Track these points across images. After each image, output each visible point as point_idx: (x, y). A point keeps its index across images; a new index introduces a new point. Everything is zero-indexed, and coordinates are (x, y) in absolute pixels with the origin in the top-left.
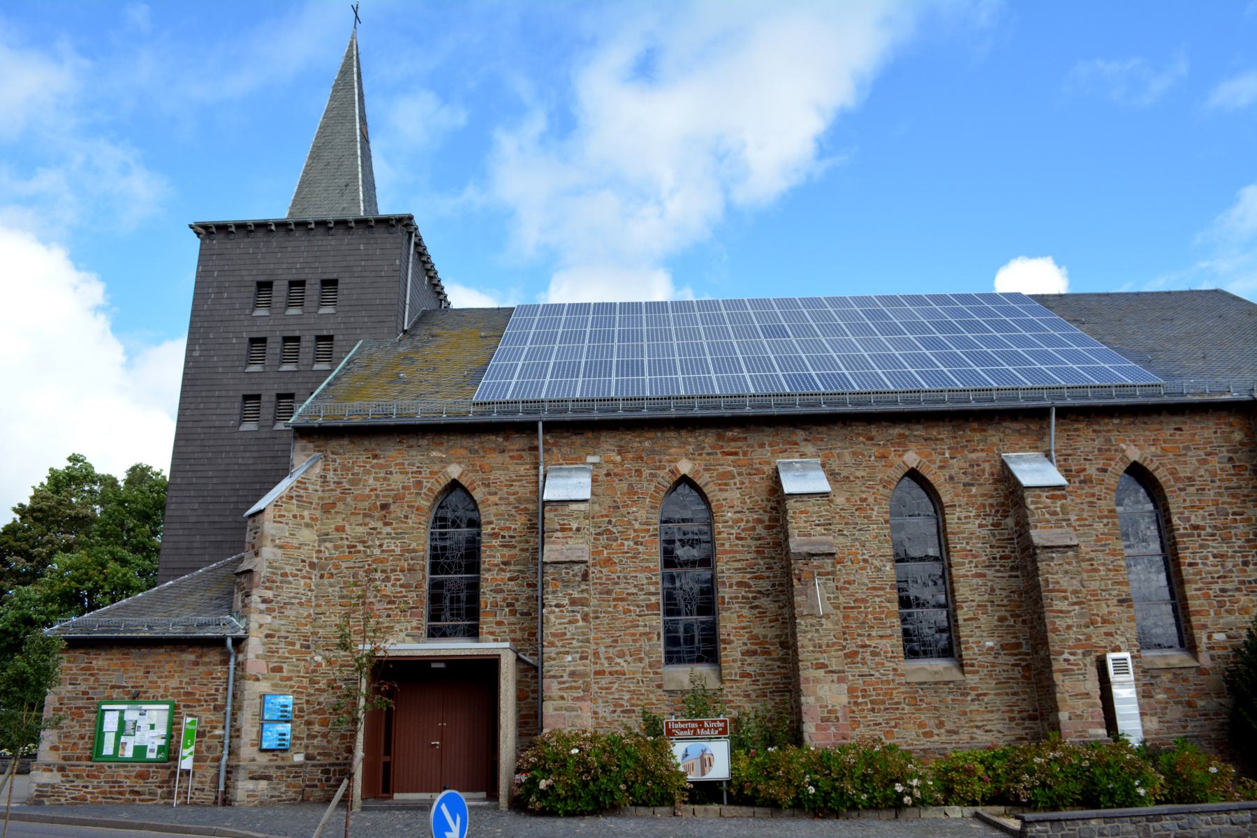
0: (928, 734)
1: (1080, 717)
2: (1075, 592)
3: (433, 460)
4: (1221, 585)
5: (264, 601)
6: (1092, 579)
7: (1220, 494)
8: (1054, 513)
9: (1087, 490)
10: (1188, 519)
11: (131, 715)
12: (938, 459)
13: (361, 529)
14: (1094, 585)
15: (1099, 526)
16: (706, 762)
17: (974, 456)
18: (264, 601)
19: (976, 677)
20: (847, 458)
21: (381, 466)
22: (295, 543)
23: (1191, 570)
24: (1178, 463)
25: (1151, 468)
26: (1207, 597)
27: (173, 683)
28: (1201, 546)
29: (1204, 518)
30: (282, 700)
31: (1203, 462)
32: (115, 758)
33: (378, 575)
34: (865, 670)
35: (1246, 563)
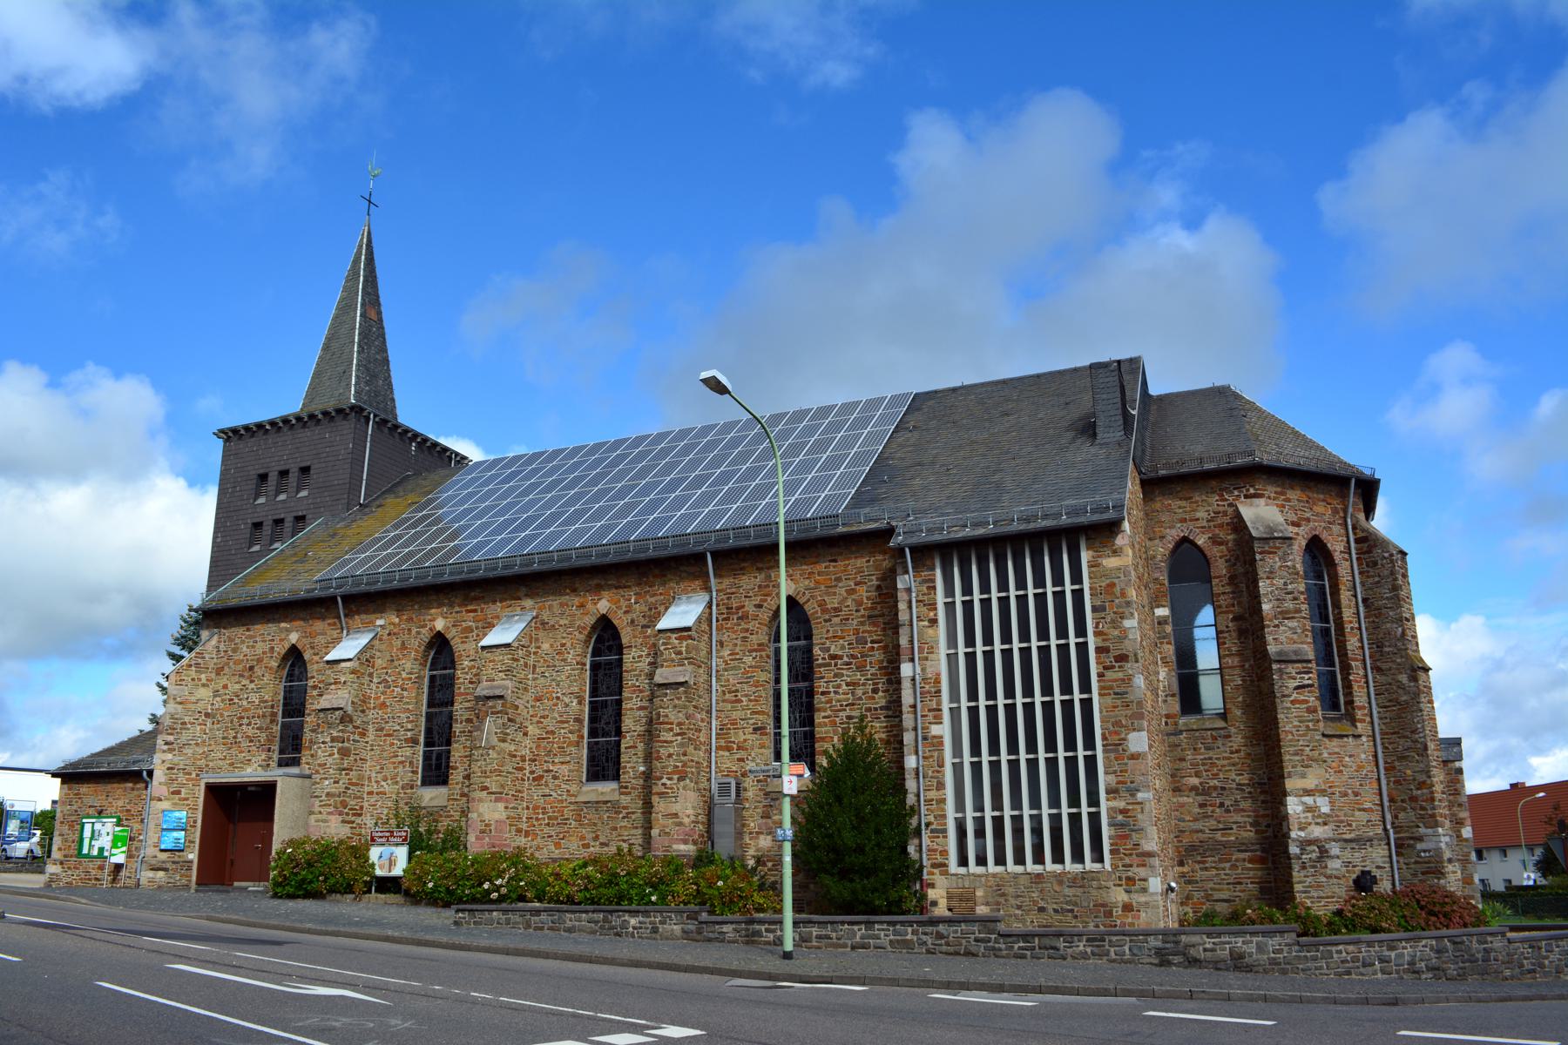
0: (586, 846)
1: (668, 834)
2: (679, 724)
3: (281, 630)
4: (848, 712)
5: (167, 743)
6: (734, 709)
7: (862, 623)
8: (680, 653)
9: (744, 626)
10: (828, 649)
11: (98, 826)
12: (623, 603)
13: (237, 686)
14: (735, 715)
15: (748, 660)
16: (392, 863)
17: (653, 600)
18: (167, 743)
19: (628, 798)
20: (557, 610)
21: (250, 637)
22: (193, 699)
23: (823, 699)
24: (828, 594)
25: (801, 601)
26: (834, 724)
27: (120, 803)
28: (836, 675)
29: (843, 647)
30: (177, 814)
31: (851, 592)
32: (88, 856)
33: (245, 721)
34: (547, 791)
35: (875, 691)
